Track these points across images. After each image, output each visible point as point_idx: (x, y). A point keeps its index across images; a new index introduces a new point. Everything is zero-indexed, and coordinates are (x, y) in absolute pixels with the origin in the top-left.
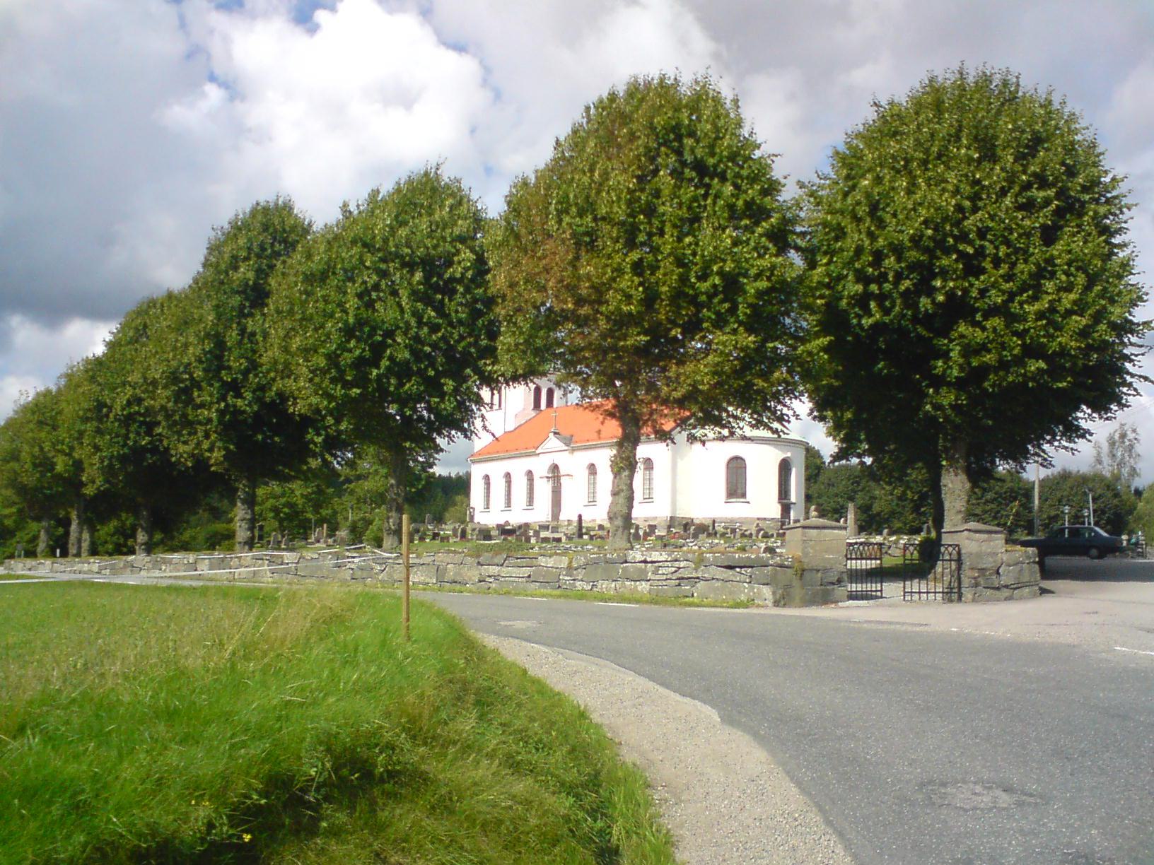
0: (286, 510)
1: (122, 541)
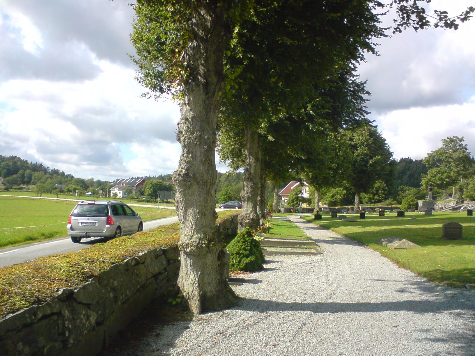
0: (447, 180)
1: (371, 196)
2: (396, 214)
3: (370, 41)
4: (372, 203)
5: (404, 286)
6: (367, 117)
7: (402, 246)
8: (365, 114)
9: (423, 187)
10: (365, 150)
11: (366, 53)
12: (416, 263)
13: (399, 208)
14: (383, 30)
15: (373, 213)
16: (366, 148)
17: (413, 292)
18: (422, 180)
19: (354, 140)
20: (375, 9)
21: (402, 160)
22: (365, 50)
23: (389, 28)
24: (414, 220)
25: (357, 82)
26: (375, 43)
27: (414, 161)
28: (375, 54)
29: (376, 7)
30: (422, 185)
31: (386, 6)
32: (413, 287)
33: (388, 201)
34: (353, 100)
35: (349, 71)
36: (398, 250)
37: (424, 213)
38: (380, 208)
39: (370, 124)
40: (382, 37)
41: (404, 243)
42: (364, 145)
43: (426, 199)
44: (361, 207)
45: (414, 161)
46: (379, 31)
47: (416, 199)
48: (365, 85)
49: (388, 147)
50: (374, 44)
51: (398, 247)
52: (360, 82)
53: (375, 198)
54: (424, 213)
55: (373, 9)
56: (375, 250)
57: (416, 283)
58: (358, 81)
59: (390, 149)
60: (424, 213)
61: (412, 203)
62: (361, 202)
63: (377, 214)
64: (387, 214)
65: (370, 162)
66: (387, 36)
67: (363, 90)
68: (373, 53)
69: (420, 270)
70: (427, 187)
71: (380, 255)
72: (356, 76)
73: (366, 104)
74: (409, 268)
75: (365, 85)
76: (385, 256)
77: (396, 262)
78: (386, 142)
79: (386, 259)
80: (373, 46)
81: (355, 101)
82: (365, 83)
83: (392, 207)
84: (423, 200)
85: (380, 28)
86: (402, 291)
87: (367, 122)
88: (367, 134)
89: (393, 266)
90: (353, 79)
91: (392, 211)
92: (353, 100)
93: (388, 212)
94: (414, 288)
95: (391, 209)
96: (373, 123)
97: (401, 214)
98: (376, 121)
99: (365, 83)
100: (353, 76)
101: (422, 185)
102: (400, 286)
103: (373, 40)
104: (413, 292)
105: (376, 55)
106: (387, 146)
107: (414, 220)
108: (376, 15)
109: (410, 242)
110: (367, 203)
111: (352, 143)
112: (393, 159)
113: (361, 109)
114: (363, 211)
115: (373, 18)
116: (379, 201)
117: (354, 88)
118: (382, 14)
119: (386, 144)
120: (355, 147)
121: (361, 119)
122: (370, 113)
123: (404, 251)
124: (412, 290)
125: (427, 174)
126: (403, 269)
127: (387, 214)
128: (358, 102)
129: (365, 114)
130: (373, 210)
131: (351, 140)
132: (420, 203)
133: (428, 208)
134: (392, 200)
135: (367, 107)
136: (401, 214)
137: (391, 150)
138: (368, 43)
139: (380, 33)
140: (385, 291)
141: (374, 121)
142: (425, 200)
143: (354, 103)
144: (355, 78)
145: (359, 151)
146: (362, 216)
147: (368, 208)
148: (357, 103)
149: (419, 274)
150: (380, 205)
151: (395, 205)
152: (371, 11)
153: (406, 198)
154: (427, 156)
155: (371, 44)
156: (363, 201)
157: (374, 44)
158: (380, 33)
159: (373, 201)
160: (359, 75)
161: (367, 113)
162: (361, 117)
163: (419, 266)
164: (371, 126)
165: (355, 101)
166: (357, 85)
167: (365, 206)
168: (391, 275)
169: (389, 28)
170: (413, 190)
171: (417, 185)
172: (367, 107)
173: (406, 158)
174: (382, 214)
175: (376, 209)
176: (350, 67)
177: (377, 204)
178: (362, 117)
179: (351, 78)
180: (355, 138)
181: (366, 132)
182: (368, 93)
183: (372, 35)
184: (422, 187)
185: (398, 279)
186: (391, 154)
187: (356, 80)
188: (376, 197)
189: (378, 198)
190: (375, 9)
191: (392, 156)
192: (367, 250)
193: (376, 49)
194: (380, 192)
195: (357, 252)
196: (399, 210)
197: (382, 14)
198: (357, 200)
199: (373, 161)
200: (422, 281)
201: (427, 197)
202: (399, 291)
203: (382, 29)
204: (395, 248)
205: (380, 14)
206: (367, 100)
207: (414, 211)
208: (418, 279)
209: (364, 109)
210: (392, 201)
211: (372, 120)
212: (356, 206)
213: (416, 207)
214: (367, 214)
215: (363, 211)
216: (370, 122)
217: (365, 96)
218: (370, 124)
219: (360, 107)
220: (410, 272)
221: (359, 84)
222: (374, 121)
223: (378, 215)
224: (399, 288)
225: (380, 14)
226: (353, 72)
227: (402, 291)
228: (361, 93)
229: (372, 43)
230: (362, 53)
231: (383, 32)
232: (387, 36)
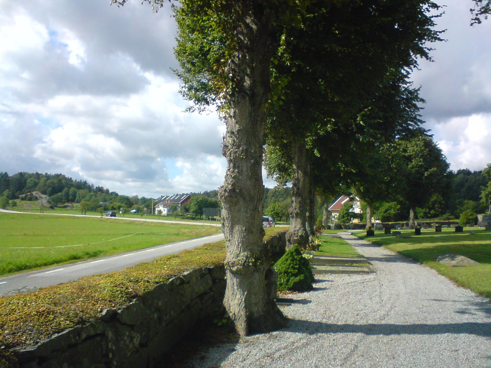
1: (427, 211)
2: (453, 230)
3: (424, 46)
4: (428, 217)
5: (464, 307)
6: (422, 126)
7: (461, 263)
8: (419, 123)
9: (483, 200)
10: (420, 162)
11: (420, 60)
12: (477, 282)
13: (457, 223)
14: (438, 33)
15: (430, 229)
16: (421, 159)
17: (473, 314)
18: (481, 193)
19: (408, 151)
20: (429, 11)
21: (460, 172)
22: (418, 56)
23: (444, 31)
24: (473, 236)
25: (410, 89)
26: (429, 48)
27: (473, 172)
28: (429, 60)
29: (430, 9)
30: (481, 198)
31: (442, 7)
32: (474, 307)
33: (445, 216)
34: (407, 109)
35: (402, 78)
36: (456, 268)
37: (484, 228)
38: (437, 223)
39: (425, 133)
40: (437, 41)
41: (462, 261)
42: (419, 157)
43: (486, 213)
44: (416, 222)
45: (473, 172)
46: (434, 34)
47: (475, 214)
48: (418, 92)
49: (444, 158)
50: (428, 49)
51: (456, 265)
52: (413, 89)
53: (431, 212)
54: (484, 228)
55: (427, 12)
56: (432, 268)
57: (477, 304)
58: (411, 88)
59: (446, 160)
60: (484, 228)
61: (471, 217)
62: (416, 217)
63: (433, 230)
64: (444, 229)
65: (426, 175)
66: (442, 40)
67: (416, 98)
68: (427, 59)
69: (482, 289)
70: (487, 200)
71: (437, 273)
72: (409, 83)
73: (421, 112)
74: (469, 288)
75: (418, 92)
76: (443, 275)
77: (454, 281)
78: (442, 153)
79: (443, 278)
80: (427, 51)
81: (409, 110)
82: (419, 90)
83: (449, 222)
84: (484, 215)
85: (434, 31)
86: (463, 312)
87: (422, 132)
88: (422, 144)
89: (451, 285)
90: (406, 86)
91: (449, 226)
92: (407, 109)
93: (445, 227)
94: (476, 310)
95: (449, 224)
96: (428, 132)
97: (459, 229)
98: (431, 130)
99: (419, 90)
100: (406, 83)
101: (481, 198)
102: (459, 306)
103: (427, 44)
104: (473, 314)
105: (430, 61)
106: (443, 157)
107: (473, 236)
108: (430, 17)
109: (469, 259)
110: (423, 218)
111: (406, 154)
112: (450, 170)
113: (415, 118)
114: (418, 227)
115: (428, 21)
116: (435, 216)
117: (407, 95)
118: (437, 16)
119: (442, 155)
120: (409, 159)
121: (415, 128)
122: (425, 122)
123: (463, 269)
124: (473, 312)
125: (487, 187)
126: (462, 289)
127: (444, 229)
128: (412, 110)
129: (419, 123)
130: (429, 225)
131: (405, 151)
132: (480, 217)
133: (488, 223)
134: (450, 214)
135: (422, 116)
136: (459, 229)
137: (448, 161)
138: (422, 48)
139: (434, 37)
140: (442, 311)
141: (429, 130)
142: (485, 214)
143: (408, 111)
144: (408, 85)
145: (413, 163)
146: (418, 232)
147: (423, 223)
148: (411, 111)
149: (481, 294)
150: (436, 220)
151: (453, 219)
152: (424, 13)
153: (464, 212)
154: (487, 167)
155: (424, 49)
156: (419, 215)
157: (428, 49)
158: (434, 37)
159: (429, 215)
160: (413, 82)
161: (422, 122)
162: (415, 126)
163: (480, 285)
164: (427, 135)
165: (409, 110)
166: (410, 92)
167: (421, 221)
168: (449, 294)
169: (444, 31)
170: (471, 203)
171: (477, 198)
172: (422, 116)
173: (464, 170)
174: (438, 230)
175: (432, 225)
176: (403, 74)
177: (433, 219)
178: (417, 127)
179: (404, 85)
180: (409, 149)
181: (421, 142)
182: (423, 100)
183: (425, 40)
184: (482, 201)
185: (457, 299)
186: (447, 166)
187: (409, 87)
188: (432, 212)
189: (434, 212)
190: (429, 11)
191: (449, 167)
192: (423, 268)
193: (430, 54)
194: (436, 206)
195: (412, 270)
196: (457, 225)
197: (437, 16)
198: (412, 215)
199: (429, 173)
200: (485, 301)
201: (488, 211)
202: (458, 312)
203: (437, 32)
204: (453, 266)
205: (435, 16)
206: (421, 108)
207: (473, 226)
208: (479, 300)
209: (418, 117)
210: (450, 215)
211: (427, 129)
212: (411, 222)
213: (475, 222)
214: (423, 230)
215: (418, 227)
216: (425, 131)
217: (419, 104)
218: (425, 133)
219: (414, 116)
220: (470, 292)
221: (413, 91)
222: (429, 130)
223: (435, 231)
224: (458, 309)
225: (435, 16)
226: (406, 79)
227: (462, 312)
228: (414, 101)
229: (425, 48)
230: (415, 59)
231: (438, 35)
232: (442, 40)
